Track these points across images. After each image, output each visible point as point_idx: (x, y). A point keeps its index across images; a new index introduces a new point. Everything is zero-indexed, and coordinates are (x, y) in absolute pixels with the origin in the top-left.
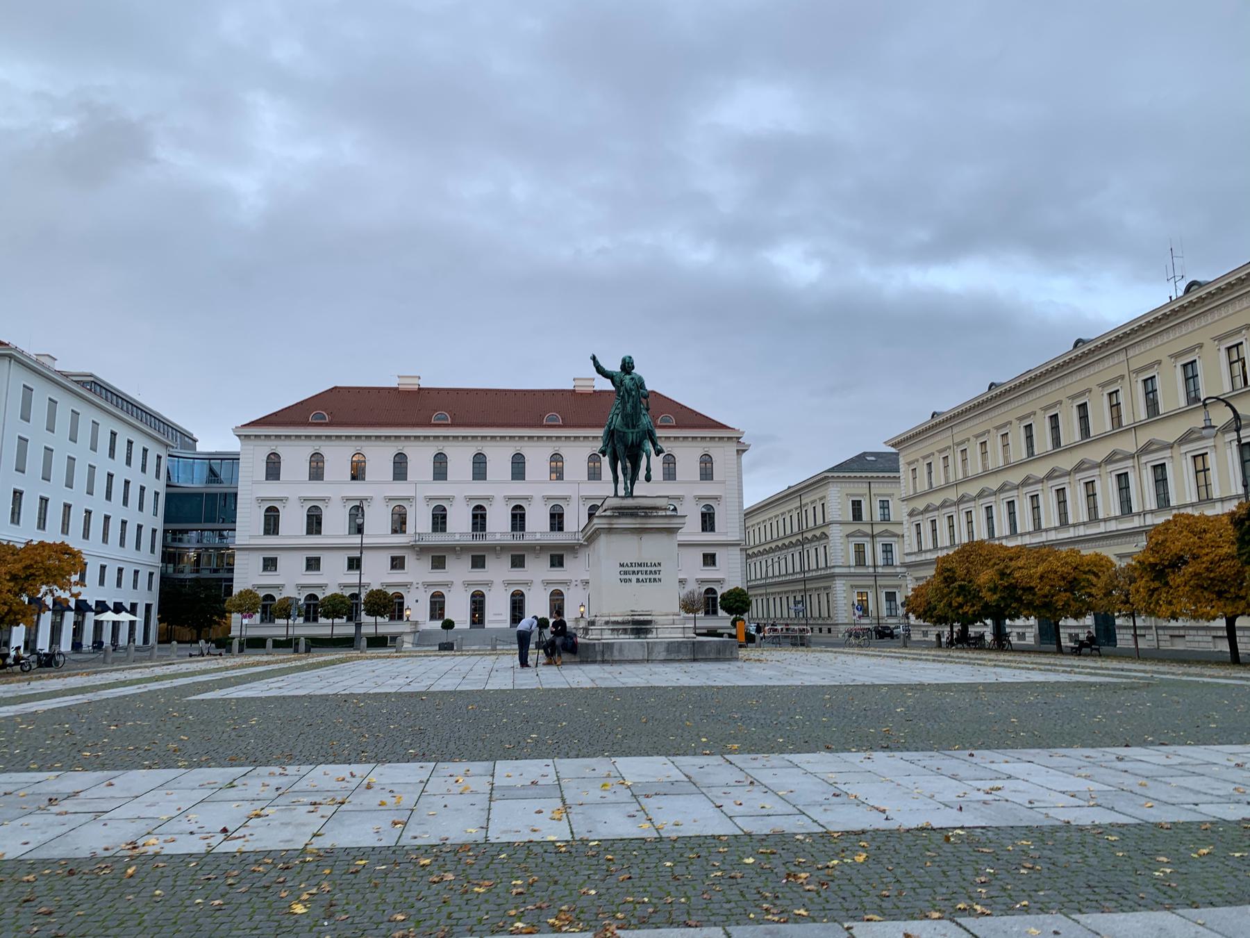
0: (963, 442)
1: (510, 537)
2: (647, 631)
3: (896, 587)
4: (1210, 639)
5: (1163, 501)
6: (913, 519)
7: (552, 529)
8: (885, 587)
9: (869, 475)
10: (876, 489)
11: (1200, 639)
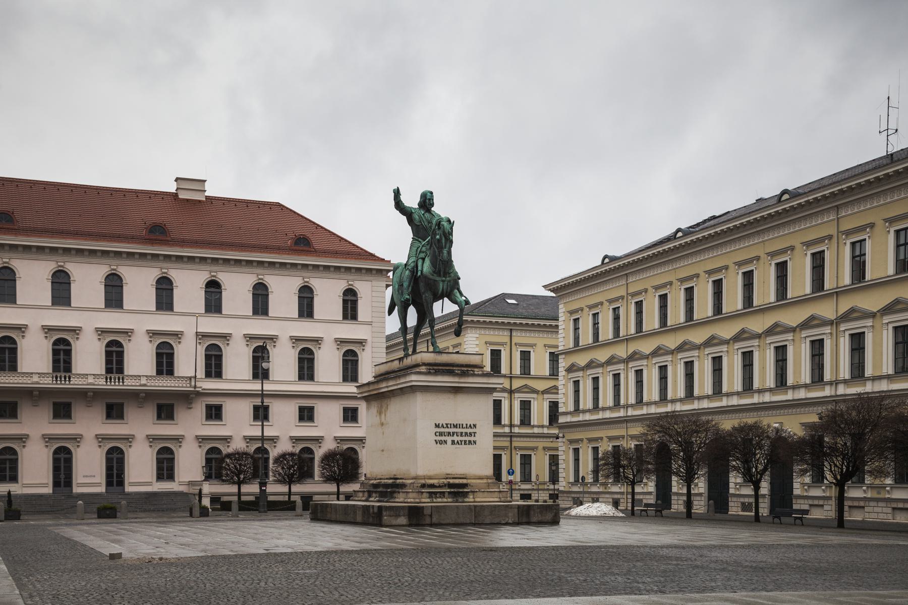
0: (639, 293)
1: (103, 382)
2: (465, 495)
3: (533, 449)
4: (890, 510)
5: (858, 371)
6: (571, 375)
7: (159, 372)
8: (521, 448)
9: (512, 321)
10: (520, 337)
11: (879, 510)
